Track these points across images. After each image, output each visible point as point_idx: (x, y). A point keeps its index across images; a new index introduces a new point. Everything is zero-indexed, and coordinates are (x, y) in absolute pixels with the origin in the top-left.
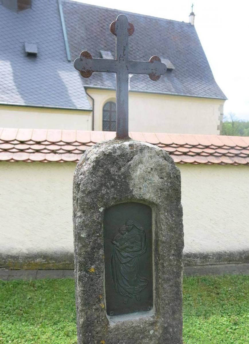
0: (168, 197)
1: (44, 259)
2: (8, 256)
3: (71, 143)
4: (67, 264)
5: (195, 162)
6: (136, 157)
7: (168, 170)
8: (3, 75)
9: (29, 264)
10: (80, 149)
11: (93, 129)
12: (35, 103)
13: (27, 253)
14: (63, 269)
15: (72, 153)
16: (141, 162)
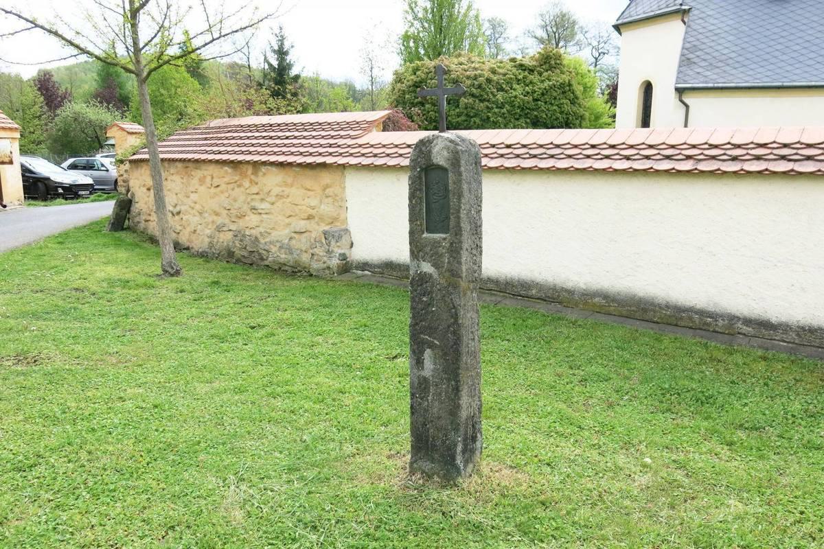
0: (453, 164)
1: (604, 299)
2: (563, 290)
3: (655, 145)
4: (633, 311)
5: (792, 170)
6: (435, 142)
7: (451, 148)
8: (716, 35)
9: (586, 303)
10: (664, 154)
11: (686, 126)
12: (768, 80)
13: (584, 288)
14: (627, 317)
15: (650, 159)
16: (437, 144)
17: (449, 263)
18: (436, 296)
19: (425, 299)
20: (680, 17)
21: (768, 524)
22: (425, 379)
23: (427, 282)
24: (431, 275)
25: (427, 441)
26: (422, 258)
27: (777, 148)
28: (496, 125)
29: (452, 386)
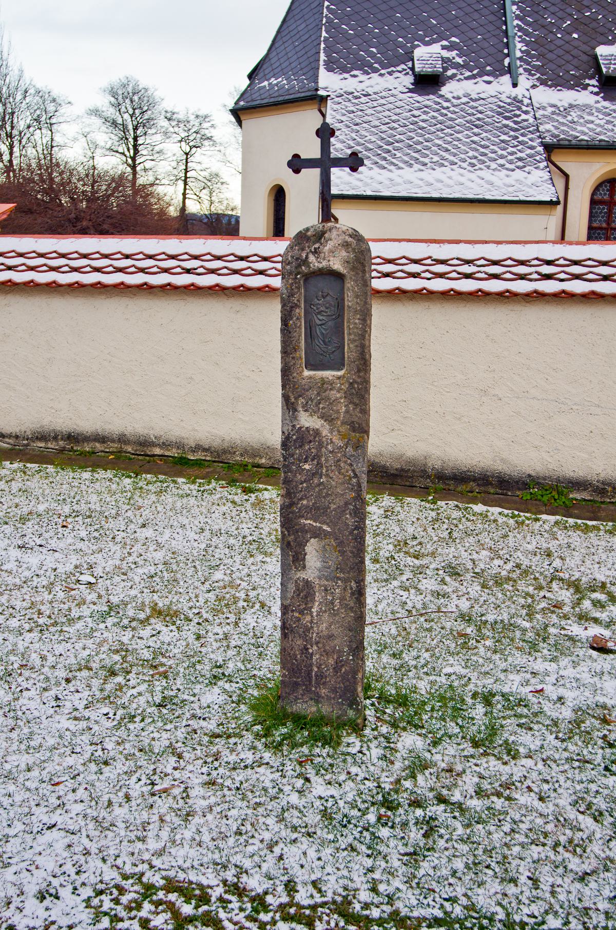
17: (347, 412)
18: (327, 460)
19: (307, 467)
20: (316, 106)
21: (149, 782)
22: (307, 583)
23: (310, 442)
24: (317, 432)
25: (309, 673)
26: (303, 407)
27: (587, 274)
28: (84, 232)
29: (351, 589)
